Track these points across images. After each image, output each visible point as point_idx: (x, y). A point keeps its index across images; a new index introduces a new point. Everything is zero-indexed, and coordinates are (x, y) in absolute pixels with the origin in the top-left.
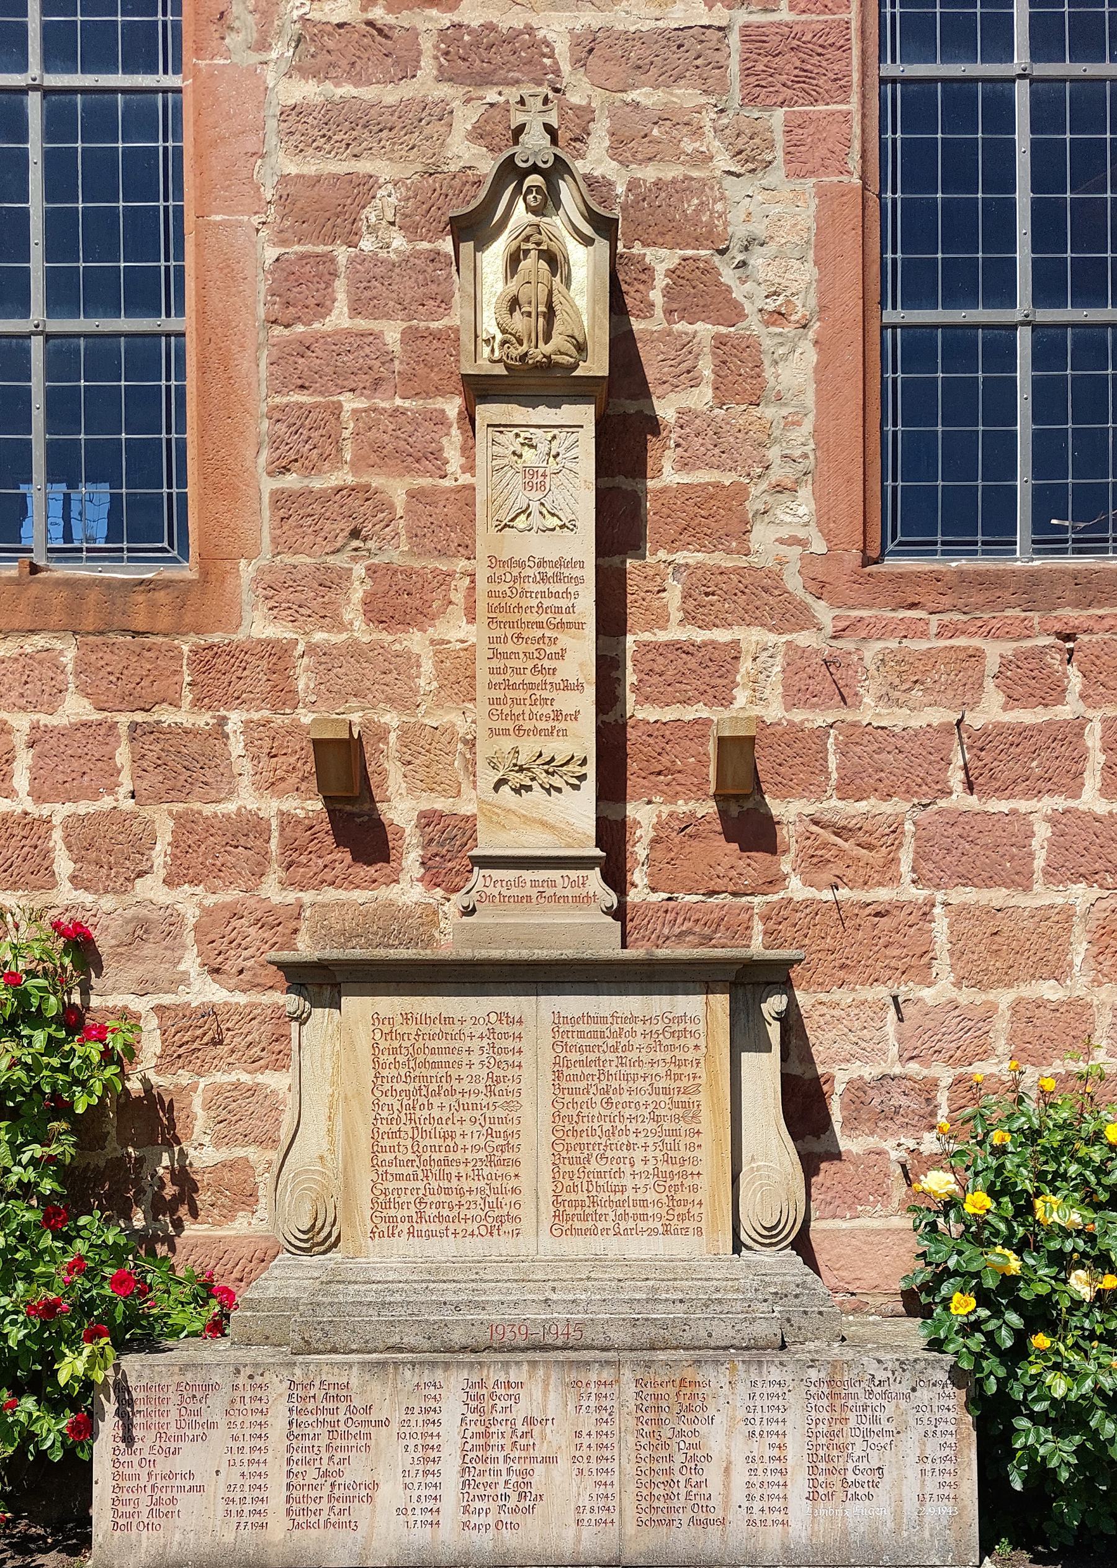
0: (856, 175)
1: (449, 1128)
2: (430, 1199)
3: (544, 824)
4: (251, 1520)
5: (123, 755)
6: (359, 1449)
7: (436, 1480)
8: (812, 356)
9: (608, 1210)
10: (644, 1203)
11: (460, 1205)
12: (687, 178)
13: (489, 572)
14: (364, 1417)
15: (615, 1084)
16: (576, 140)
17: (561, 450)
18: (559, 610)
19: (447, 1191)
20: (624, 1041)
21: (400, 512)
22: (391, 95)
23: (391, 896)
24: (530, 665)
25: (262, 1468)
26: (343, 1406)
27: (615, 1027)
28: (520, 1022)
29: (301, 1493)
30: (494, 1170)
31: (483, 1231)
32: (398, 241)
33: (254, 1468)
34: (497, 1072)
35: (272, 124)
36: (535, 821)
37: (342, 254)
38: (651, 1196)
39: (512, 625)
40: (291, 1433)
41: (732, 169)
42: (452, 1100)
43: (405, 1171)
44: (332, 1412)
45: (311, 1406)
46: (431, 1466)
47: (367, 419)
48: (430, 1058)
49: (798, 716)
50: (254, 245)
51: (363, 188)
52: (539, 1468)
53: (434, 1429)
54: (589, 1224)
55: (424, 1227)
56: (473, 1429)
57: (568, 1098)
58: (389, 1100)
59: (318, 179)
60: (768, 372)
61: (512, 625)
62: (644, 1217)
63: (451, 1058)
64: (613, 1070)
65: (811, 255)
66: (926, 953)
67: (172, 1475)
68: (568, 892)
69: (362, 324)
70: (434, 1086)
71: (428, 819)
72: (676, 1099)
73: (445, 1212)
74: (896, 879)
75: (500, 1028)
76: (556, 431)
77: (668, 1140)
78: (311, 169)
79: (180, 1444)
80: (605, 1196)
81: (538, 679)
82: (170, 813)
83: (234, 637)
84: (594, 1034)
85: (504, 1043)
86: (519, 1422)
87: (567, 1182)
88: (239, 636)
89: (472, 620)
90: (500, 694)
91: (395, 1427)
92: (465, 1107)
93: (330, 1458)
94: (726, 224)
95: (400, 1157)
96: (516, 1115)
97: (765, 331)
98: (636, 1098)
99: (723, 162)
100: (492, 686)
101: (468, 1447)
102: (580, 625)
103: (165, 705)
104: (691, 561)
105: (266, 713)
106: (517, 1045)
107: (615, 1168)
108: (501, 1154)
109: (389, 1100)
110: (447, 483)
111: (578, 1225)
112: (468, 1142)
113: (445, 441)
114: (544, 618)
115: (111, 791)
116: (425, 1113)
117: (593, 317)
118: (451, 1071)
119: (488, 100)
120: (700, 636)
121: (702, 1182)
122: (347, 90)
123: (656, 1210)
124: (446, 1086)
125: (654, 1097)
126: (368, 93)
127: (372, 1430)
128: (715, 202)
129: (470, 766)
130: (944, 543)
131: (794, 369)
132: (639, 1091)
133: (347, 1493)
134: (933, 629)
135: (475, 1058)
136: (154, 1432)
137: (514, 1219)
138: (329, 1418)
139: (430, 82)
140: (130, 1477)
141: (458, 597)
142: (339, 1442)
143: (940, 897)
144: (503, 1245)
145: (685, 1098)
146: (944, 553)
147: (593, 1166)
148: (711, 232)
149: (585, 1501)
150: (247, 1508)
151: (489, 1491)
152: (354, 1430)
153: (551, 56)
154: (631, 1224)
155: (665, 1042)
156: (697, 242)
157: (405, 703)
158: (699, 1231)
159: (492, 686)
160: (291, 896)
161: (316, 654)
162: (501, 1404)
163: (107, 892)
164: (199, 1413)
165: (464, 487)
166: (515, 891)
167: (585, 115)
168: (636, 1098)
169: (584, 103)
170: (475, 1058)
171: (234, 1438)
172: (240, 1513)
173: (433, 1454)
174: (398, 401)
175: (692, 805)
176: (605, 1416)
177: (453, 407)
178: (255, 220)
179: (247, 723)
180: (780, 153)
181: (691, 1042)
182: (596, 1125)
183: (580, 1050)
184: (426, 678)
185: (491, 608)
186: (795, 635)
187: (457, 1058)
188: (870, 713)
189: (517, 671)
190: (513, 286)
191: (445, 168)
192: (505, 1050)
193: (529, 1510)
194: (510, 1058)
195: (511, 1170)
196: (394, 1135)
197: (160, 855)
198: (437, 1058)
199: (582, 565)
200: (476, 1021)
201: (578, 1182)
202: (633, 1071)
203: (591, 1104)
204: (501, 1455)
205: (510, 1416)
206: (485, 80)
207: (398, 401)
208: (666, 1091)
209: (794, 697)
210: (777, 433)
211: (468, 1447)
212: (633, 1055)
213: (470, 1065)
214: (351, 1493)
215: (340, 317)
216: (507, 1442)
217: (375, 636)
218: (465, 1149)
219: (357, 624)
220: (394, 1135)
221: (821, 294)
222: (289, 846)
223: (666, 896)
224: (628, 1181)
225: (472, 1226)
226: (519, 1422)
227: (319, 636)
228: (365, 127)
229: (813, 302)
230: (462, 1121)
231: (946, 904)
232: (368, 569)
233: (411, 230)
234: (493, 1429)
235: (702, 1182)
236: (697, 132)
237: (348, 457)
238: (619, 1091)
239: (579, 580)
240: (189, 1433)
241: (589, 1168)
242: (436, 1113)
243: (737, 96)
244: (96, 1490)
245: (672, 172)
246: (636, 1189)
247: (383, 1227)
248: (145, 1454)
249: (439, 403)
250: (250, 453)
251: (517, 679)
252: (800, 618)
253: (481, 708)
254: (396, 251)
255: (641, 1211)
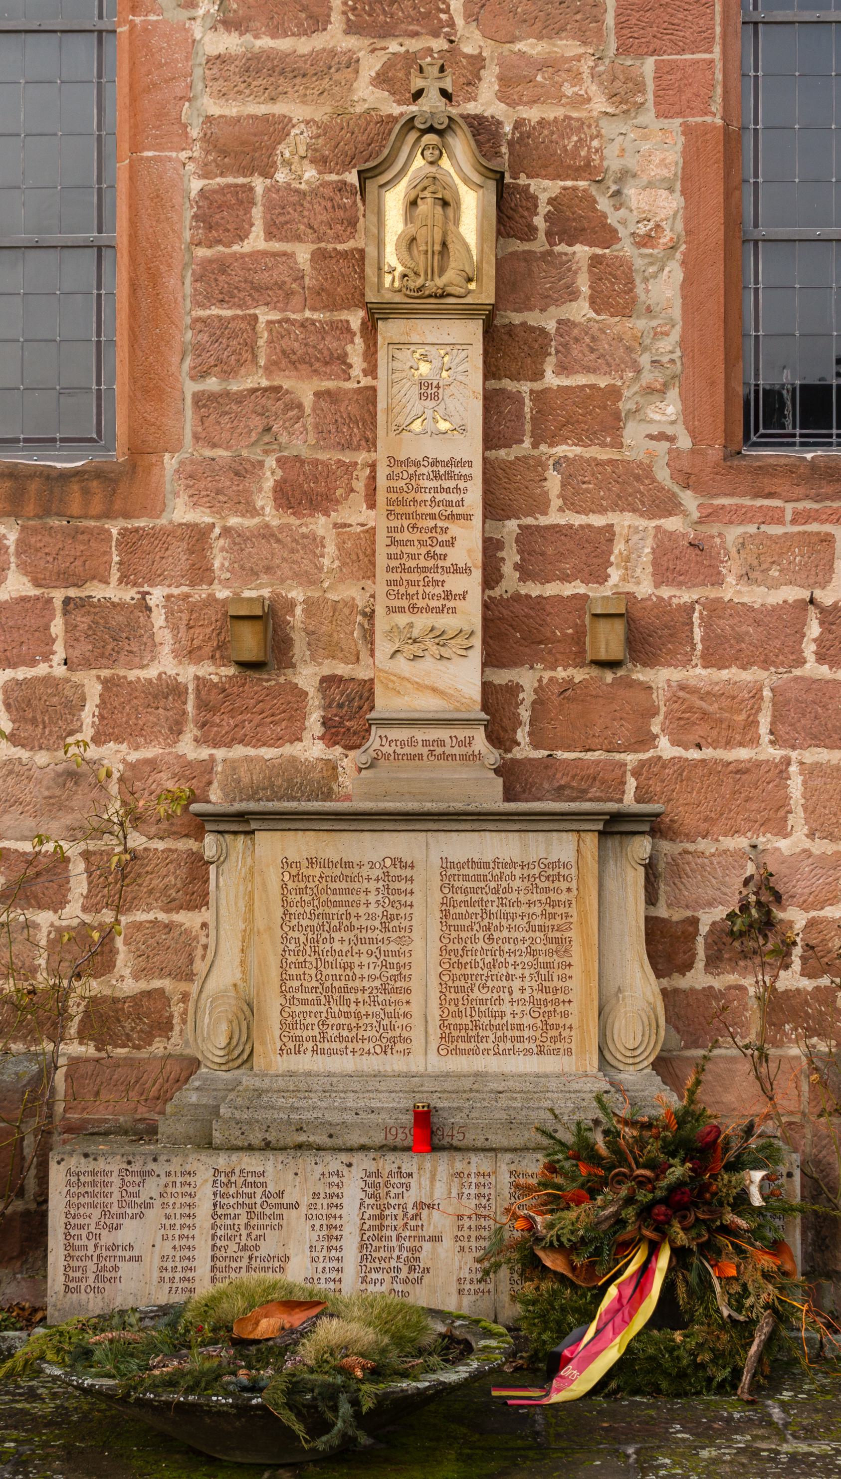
0: (718, 116)
1: (349, 959)
2: (331, 1021)
3: (434, 690)
4: (181, 1285)
5: (57, 627)
6: (273, 1228)
7: (338, 1254)
8: (679, 275)
9: (489, 1033)
10: (520, 1027)
11: (358, 1027)
12: (568, 118)
13: (388, 471)
14: (278, 1201)
15: (496, 922)
16: (469, 84)
17: (453, 366)
18: (450, 504)
19: (347, 1015)
20: (504, 884)
21: (308, 410)
22: (304, 46)
23: (295, 753)
24: (423, 551)
25: (191, 1242)
26: (259, 1191)
27: (497, 871)
28: (412, 867)
29: (223, 1264)
30: (387, 997)
31: (378, 1050)
32: (310, 173)
33: (184, 1242)
34: (391, 911)
35: (198, 72)
36: (427, 687)
37: (259, 184)
38: (527, 1021)
39: (408, 516)
40: (215, 1213)
41: (609, 110)
42: (351, 935)
43: (310, 996)
44: (251, 1196)
45: (232, 1190)
46: (334, 1243)
47: (279, 330)
48: (333, 898)
49: (666, 592)
50: (181, 178)
51: (279, 128)
52: (427, 1246)
53: (338, 1212)
54: (472, 1045)
55: (326, 1045)
56: (370, 1212)
57: (454, 934)
58: (296, 934)
59: (238, 120)
60: (639, 289)
61: (408, 516)
62: (520, 1039)
63: (350, 898)
64: (494, 910)
65: (678, 186)
66: (782, 806)
67: (115, 1247)
68: (456, 751)
69: (277, 246)
70: (335, 922)
71: (328, 682)
72: (550, 935)
73: (345, 1033)
74: (755, 741)
75: (394, 872)
76: (448, 348)
77: (543, 971)
78: (232, 110)
79: (121, 1221)
80: (486, 1021)
81: (430, 563)
82: (98, 677)
83: (158, 521)
84: (478, 878)
85: (397, 885)
86: (410, 1206)
87: (452, 1008)
88: (163, 521)
89: (372, 506)
90: (396, 576)
91: (303, 1209)
92: (362, 941)
93: (249, 1235)
94: (602, 159)
95: (306, 984)
96: (407, 949)
97: (636, 252)
98: (515, 934)
99: (600, 104)
100: (389, 569)
101: (366, 1227)
102: (468, 517)
103: (95, 582)
104: (571, 455)
105: (185, 589)
106: (409, 886)
107: (496, 996)
108: (395, 983)
109: (296, 934)
110: (351, 385)
111: (462, 1046)
112: (365, 972)
113: (349, 348)
114: (436, 510)
115: (46, 658)
116: (328, 946)
117: (481, 252)
118: (350, 910)
119: (390, 50)
120: (578, 520)
121: (573, 1008)
122: (265, 42)
123: (532, 1033)
124: (346, 923)
125: (531, 934)
126: (284, 44)
127: (285, 1212)
128: (592, 139)
129: (369, 636)
130: (802, 436)
131: (664, 288)
132: (516, 928)
133: (263, 1264)
134: (789, 517)
135: (372, 898)
136: (99, 1210)
137: (405, 1040)
138: (247, 1201)
139: (340, 35)
140: (79, 1248)
141: (360, 486)
142: (255, 1222)
143: (794, 755)
144: (395, 1063)
145: (558, 935)
146: (803, 444)
147: (476, 994)
148: (588, 165)
149: (465, 1273)
150: (178, 1275)
151: (383, 1265)
152: (268, 1212)
153: (447, 11)
154: (509, 1045)
155: (541, 885)
156: (577, 172)
157: (310, 579)
158: (569, 1052)
159: (389, 569)
160: (204, 753)
161: (231, 536)
162: (393, 1191)
163: (41, 748)
164: (137, 1195)
165: (366, 388)
166: (408, 750)
167: (477, 62)
168: (515, 934)
169: (476, 52)
170: (372, 898)
171: (167, 1217)
172: (172, 1280)
173: (336, 1233)
174: (308, 314)
175: (571, 671)
176: (484, 1202)
177: (355, 319)
178: (183, 155)
179: (168, 598)
180: (650, 96)
181: (564, 885)
182: (478, 959)
183: (465, 891)
184: (329, 558)
185: (389, 502)
186: (663, 521)
187: (356, 898)
188: (732, 590)
189: (412, 557)
190: (412, 230)
191: (352, 110)
192: (398, 891)
193: (419, 1281)
194: (402, 898)
195: (403, 997)
196: (299, 965)
197: (88, 716)
198: (338, 898)
199: (470, 464)
200: (372, 865)
201: (462, 1008)
202: (512, 910)
203: (474, 940)
204: (394, 1234)
205: (401, 1201)
206: (387, 32)
207: (308, 314)
208: (541, 928)
209: (662, 575)
210: (648, 341)
211: (366, 1227)
212: (513, 896)
213: (368, 904)
214: (266, 1264)
215: (256, 241)
216: (399, 1223)
217: (284, 521)
218: (362, 978)
219: (268, 510)
220: (299, 965)
221: (687, 221)
222: (203, 705)
223: (547, 753)
224: (507, 1008)
225: (368, 1046)
226: (410, 1206)
227: (234, 521)
228: (281, 74)
229: (680, 226)
230: (359, 953)
231: (802, 763)
232: (278, 460)
233: (321, 162)
234: (387, 1212)
235: (573, 1008)
236: (577, 77)
237: (262, 362)
238: (500, 928)
239: (467, 478)
240: (129, 1211)
241: (472, 996)
242: (337, 946)
243: (613, 46)
244: (51, 1258)
245: (552, 113)
246: (514, 1014)
247: (291, 1045)
248: (92, 1228)
249: (344, 315)
250: (175, 360)
251: (412, 564)
252: (667, 505)
253: (381, 588)
254: (307, 182)
255: (518, 1033)
